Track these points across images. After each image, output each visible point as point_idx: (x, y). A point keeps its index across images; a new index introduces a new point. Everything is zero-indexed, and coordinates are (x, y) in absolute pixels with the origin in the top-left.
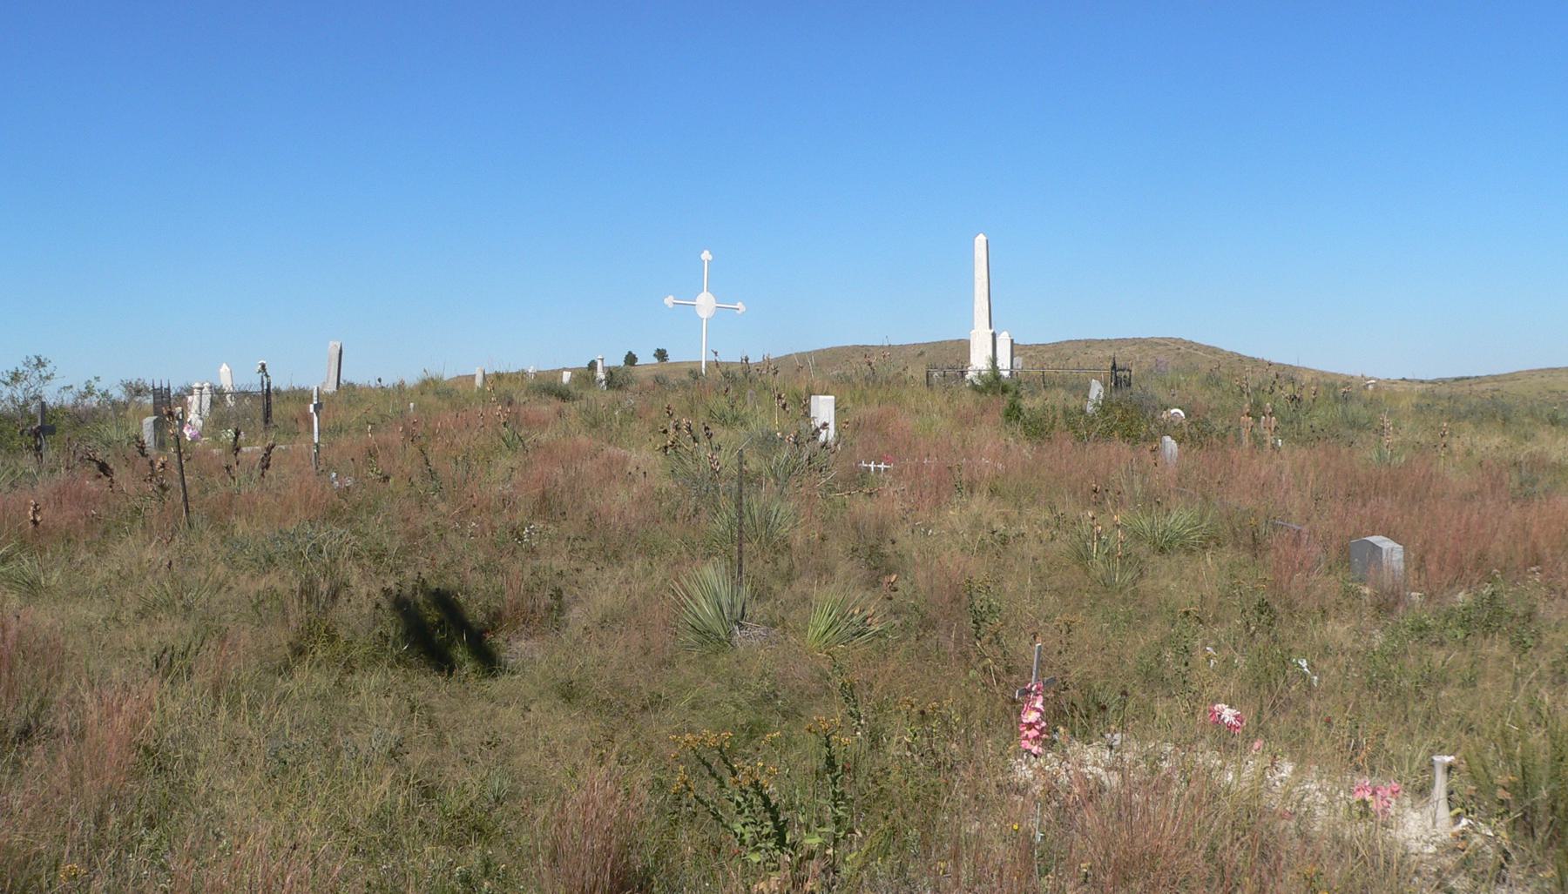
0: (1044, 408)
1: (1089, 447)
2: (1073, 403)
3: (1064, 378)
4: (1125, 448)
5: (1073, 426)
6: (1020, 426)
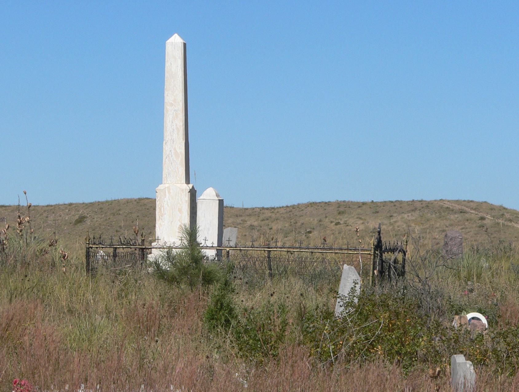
0: (269, 307)
1: (338, 369)
2: (314, 301)
3: (301, 262)
4: (391, 371)
5: (312, 337)
6: (230, 337)
